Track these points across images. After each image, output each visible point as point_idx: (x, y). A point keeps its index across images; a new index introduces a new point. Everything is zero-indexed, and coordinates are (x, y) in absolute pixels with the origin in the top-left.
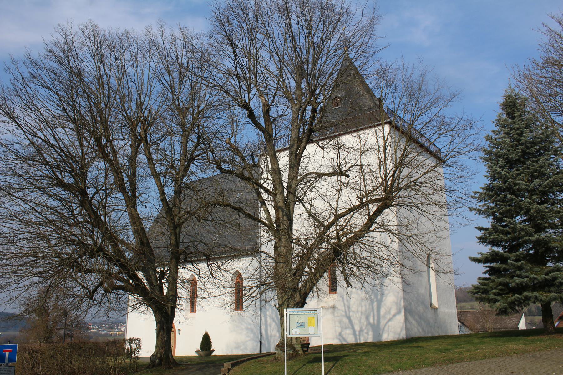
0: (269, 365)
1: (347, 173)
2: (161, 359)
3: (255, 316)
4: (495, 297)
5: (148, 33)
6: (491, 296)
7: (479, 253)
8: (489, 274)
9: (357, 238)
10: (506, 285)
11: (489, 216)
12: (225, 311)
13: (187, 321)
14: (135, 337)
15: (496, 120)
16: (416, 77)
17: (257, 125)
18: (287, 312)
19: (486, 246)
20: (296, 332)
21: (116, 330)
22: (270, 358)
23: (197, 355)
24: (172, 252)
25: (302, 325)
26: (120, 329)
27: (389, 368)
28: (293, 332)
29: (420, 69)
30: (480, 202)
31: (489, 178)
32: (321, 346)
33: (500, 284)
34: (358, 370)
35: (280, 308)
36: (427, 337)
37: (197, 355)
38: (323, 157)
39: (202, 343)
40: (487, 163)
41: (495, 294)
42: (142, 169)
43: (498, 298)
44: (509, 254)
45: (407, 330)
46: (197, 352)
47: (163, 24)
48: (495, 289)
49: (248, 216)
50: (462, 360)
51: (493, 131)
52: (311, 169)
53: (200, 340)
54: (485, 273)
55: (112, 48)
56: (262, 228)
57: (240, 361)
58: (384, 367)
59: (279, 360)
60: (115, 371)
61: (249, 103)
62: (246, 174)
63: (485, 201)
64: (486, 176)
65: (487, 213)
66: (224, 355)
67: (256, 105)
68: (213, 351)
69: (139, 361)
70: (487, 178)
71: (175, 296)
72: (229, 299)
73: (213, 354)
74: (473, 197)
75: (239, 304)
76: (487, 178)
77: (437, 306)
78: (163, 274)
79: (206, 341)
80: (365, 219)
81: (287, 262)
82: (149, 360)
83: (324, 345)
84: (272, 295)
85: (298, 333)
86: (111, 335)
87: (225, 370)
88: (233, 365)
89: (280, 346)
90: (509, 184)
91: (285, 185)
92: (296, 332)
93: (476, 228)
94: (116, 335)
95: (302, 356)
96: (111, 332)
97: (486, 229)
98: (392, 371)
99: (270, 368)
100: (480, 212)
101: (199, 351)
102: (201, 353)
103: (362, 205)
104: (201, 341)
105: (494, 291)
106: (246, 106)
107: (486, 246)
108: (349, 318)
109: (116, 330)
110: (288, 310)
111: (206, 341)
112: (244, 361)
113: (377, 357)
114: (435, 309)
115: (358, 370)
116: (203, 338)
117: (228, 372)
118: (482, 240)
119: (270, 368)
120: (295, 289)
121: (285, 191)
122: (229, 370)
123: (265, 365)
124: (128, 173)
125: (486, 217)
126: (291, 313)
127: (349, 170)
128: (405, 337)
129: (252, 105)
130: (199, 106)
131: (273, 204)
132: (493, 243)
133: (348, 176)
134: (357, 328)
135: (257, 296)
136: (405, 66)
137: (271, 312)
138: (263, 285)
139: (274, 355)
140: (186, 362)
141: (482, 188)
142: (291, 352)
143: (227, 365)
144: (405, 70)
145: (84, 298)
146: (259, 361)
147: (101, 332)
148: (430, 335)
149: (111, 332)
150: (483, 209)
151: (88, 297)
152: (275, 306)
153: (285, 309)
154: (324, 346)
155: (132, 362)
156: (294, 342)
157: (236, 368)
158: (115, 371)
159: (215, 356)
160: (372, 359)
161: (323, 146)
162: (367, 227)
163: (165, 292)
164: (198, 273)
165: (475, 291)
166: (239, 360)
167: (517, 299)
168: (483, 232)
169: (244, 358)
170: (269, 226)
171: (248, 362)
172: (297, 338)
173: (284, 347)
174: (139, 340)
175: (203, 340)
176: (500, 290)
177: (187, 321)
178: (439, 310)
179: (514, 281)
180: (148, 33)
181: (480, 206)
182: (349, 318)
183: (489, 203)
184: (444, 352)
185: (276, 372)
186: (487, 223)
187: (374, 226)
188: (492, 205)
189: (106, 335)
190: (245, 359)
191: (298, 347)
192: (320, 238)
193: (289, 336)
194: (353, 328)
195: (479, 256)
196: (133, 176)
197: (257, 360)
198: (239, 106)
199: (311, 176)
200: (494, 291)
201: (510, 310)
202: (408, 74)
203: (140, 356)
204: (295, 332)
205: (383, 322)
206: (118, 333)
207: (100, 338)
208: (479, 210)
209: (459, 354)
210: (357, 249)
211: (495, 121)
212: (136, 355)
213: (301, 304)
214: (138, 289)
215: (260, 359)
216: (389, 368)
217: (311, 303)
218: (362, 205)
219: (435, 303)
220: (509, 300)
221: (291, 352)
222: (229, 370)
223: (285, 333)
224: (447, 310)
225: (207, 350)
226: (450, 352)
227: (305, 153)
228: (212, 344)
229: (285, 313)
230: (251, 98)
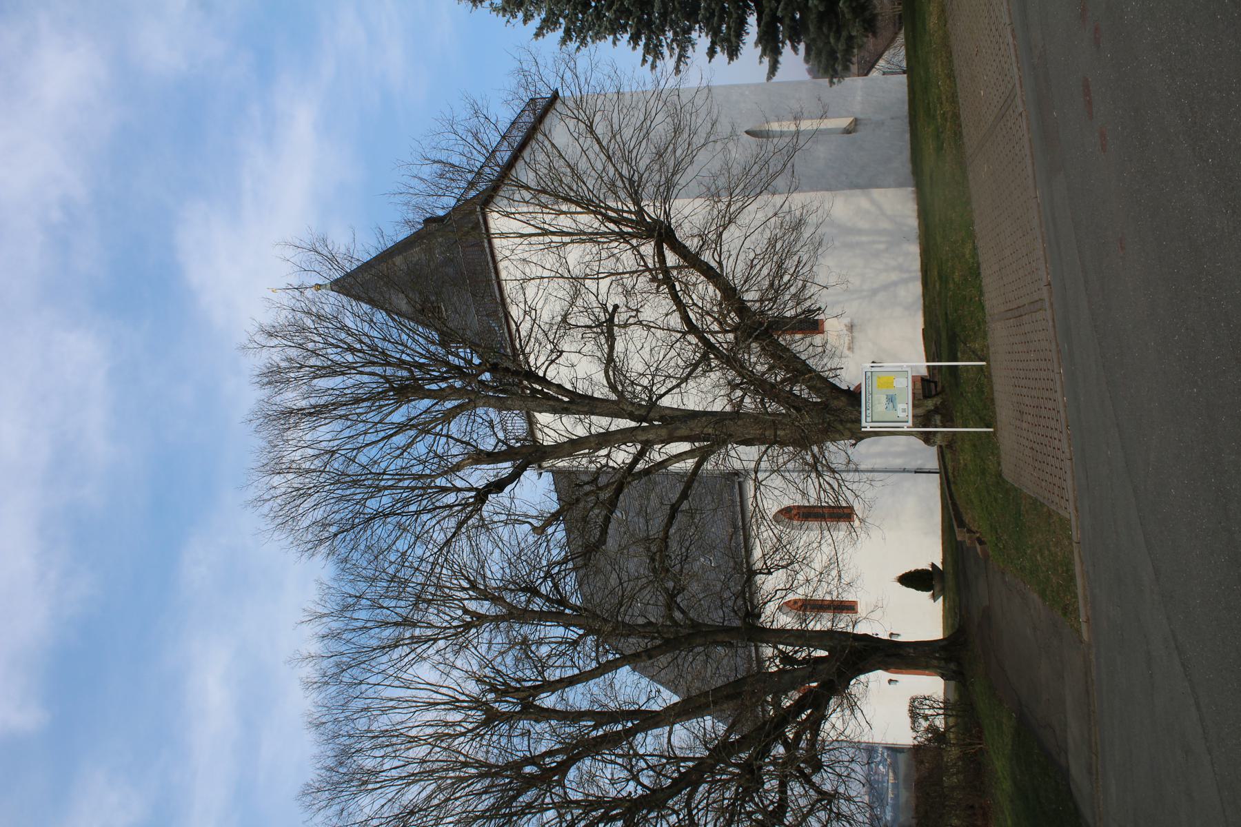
0: (961, 458)
1: (610, 309)
2: (948, 660)
3: (873, 483)
4: (842, 39)
5: (308, 685)
6: (841, 46)
7: (761, 62)
8: (799, 43)
9: (730, 293)
10: (821, 17)
11: (690, 40)
12: (863, 535)
13: (880, 605)
14: (907, 708)
15: (504, 16)
16: (427, 171)
17: (515, 476)
18: (867, 426)
19: (744, 44)
20: (904, 410)
21: (885, 784)
22: (948, 456)
23: (941, 568)
24: (748, 640)
25: (891, 399)
26: (883, 776)
27: (969, 246)
28: (902, 415)
29: (418, 167)
30: (662, 54)
31: (618, 36)
32: (928, 367)
33: (820, 28)
34: (971, 300)
35: (859, 436)
36: (912, 143)
37: (941, 599)
38: (579, 352)
39: (917, 589)
40: (589, 39)
41: (838, 39)
42: (578, 698)
43: (844, 34)
44: (765, 12)
45: (900, 185)
46: (934, 598)
47: (298, 656)
48: (828, 37)
49: (684, 495)
50: (956, 116)
51: (525, 22)
52: (600, 377)
53: (912, 592)
54: (795, 49)
55: (345, 754)
56: (708, 466)
57: (954, 510)
58: (967, 256)
59: (953, 439)
60: (970, 744)
61: (476, 489)
62: (605, 495)
63: (662, 46)
64: (614, 43)
65: (683, 42)
66: (943, 544)
67: (479, 476)
68: (933, 565)
69: (952, 701)
70: (619, 40)
71: (830, 634)
72: (841, 532)
73: (940, 567)
74: (653, 67)
75: (841, 514)
76: (619, 40)
77: (851, 119)
78: (786, 659)
79: (914, 580)
80: (695, 277)
81: (775, 422)
82: (952, 683)
83: (928, 361)
84: (836, 452)
85: (905, 406)
86: (896, 797)
87: (970, 538)
88: (961, 524)
89: (927, 438)
90: (633, 6)
91: (633, 424)
92: (904, 410)
93: (710, 61)
94: (895, 786)
95: (944, 397)
96: (890, 795)
97: (713, 43)
98: (974, 243)
99: (966, 457)
100: (681, 57)
101: (933, 594)
102: (937, 588)
103: (668, 281)
104: (914, 590)
105: (832, 41)
106: (482, 495)
107: (744, 44)
108: (874, 292)
109: (885, 784)
110: (864, 424)
111: (914, 580)
112: (954, 504)
113: (950, 264)
114: (856, 122)
115: (971, 300)
116: (908, 586)
117: (974, 533)
118: (733, 53)
119: (966, 457)
120: (824, 407)
121: (644, 424)
122: (969, 531)
123: (962, 466)
124: (590, 726)
125: (693, 45)
126: (869, 419)
127: (605, 305)
128: (911, 189)
129: (481, 484)
130: (464, 589)
131: (660, 446)
132: (739, 28)
133: (616, 307)
134: (894, 276)
135: (837, 480)
136: (403, 190)
137: (865, 451)
138: (816, 467)
139: (944, 449)
140: (957, 619)
141: (634, 48)
142: (938, 418)
143: (961, 536)
144: (411, 191)
145: (831, 810)
146: (954, 477)
147: (889, 818)
148: (907, 136)
149: (890, 795)
150: (677, 51)
151: (830, 803)
152: (854, 445)
153: (863, 429)
154: (928, 361)
155: (954, 713)
156: (921, 411)
157: (967, 518)
158: (970, 744)
159: (943, 563)
160: (954, 273)
161: (558, 351)
162: (710, 274)
163: (824, 653)
164: (784, 592)
165: (831, 72)
166: (952, 513)
167: (847, 4)
168: (718, 49)
169: (947, 504)
170: (703, 455)
171: (956, 496)
172: (914, 406)
173: (930, 432)
174: (913, 700)
175: (912, 587)
176: (830, 29)
177: (880, 605)
178: (860, 116)
179: (816, 6)
180: (308, 685)
181: (671, 56)
182: (874, 292)
183: (666, 39)
184: (943, 143)
185: (974, 446)
186: (701, 40)
187: (707, 257)
188: (670, 34)
189: (895, 807)
190: (950, 502)
191: (930, 404)
192: (730, 360)
193: (910, 423)
194: (895, 284)
195: (766, 60)
196: (603, 717)
197: (952, 479)
198: (481, 509)
199: (612, 377)
200: (832, 41)
201: (867, 14)
202: (421, 186)
203: (941, 698)
204: (904, 410)
205: (885, 225)
206: (891, 781)
207: (902, 819)
208: (679, 60)
209: (946, 120)
210: (750, 296)
211: (505, 19)
212: (941, 705)
213: (853, 397)
214: (817, 704)
215: (950, 474)
216: (969, 246)
217: (848, 378)
218: (668, 281)
219: (844, 122)
220: (848, 16)
221: (938, 418)
222: (969, 531)
223: (906, 429)
224: (859, 98)
225: (932, 579)
226: (942, 132)
227: (569, 386)
228: (920, 568)
229: (868, 429)
230: (469, 486)
